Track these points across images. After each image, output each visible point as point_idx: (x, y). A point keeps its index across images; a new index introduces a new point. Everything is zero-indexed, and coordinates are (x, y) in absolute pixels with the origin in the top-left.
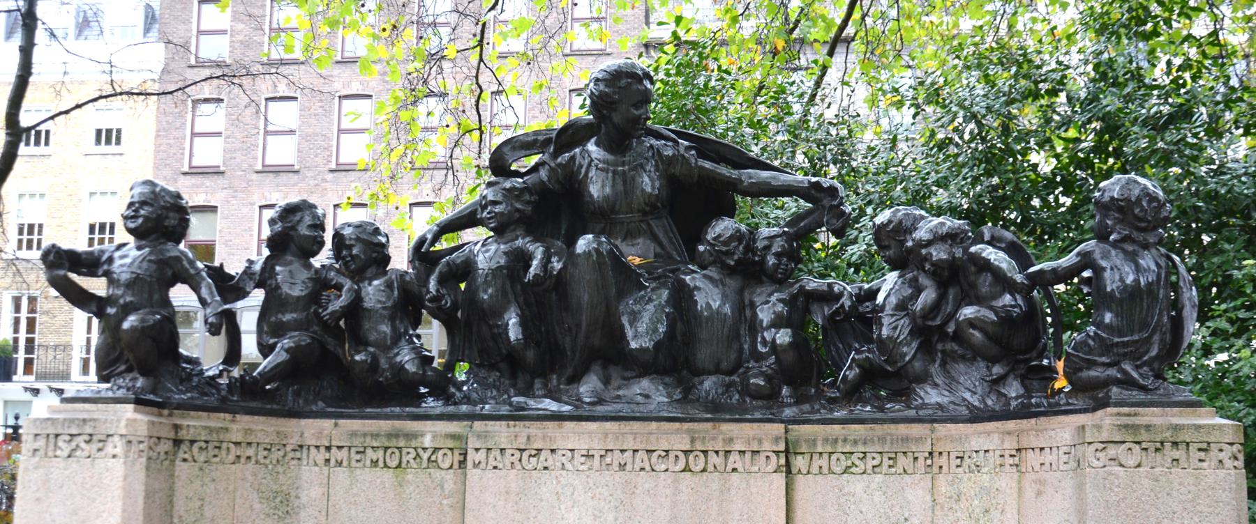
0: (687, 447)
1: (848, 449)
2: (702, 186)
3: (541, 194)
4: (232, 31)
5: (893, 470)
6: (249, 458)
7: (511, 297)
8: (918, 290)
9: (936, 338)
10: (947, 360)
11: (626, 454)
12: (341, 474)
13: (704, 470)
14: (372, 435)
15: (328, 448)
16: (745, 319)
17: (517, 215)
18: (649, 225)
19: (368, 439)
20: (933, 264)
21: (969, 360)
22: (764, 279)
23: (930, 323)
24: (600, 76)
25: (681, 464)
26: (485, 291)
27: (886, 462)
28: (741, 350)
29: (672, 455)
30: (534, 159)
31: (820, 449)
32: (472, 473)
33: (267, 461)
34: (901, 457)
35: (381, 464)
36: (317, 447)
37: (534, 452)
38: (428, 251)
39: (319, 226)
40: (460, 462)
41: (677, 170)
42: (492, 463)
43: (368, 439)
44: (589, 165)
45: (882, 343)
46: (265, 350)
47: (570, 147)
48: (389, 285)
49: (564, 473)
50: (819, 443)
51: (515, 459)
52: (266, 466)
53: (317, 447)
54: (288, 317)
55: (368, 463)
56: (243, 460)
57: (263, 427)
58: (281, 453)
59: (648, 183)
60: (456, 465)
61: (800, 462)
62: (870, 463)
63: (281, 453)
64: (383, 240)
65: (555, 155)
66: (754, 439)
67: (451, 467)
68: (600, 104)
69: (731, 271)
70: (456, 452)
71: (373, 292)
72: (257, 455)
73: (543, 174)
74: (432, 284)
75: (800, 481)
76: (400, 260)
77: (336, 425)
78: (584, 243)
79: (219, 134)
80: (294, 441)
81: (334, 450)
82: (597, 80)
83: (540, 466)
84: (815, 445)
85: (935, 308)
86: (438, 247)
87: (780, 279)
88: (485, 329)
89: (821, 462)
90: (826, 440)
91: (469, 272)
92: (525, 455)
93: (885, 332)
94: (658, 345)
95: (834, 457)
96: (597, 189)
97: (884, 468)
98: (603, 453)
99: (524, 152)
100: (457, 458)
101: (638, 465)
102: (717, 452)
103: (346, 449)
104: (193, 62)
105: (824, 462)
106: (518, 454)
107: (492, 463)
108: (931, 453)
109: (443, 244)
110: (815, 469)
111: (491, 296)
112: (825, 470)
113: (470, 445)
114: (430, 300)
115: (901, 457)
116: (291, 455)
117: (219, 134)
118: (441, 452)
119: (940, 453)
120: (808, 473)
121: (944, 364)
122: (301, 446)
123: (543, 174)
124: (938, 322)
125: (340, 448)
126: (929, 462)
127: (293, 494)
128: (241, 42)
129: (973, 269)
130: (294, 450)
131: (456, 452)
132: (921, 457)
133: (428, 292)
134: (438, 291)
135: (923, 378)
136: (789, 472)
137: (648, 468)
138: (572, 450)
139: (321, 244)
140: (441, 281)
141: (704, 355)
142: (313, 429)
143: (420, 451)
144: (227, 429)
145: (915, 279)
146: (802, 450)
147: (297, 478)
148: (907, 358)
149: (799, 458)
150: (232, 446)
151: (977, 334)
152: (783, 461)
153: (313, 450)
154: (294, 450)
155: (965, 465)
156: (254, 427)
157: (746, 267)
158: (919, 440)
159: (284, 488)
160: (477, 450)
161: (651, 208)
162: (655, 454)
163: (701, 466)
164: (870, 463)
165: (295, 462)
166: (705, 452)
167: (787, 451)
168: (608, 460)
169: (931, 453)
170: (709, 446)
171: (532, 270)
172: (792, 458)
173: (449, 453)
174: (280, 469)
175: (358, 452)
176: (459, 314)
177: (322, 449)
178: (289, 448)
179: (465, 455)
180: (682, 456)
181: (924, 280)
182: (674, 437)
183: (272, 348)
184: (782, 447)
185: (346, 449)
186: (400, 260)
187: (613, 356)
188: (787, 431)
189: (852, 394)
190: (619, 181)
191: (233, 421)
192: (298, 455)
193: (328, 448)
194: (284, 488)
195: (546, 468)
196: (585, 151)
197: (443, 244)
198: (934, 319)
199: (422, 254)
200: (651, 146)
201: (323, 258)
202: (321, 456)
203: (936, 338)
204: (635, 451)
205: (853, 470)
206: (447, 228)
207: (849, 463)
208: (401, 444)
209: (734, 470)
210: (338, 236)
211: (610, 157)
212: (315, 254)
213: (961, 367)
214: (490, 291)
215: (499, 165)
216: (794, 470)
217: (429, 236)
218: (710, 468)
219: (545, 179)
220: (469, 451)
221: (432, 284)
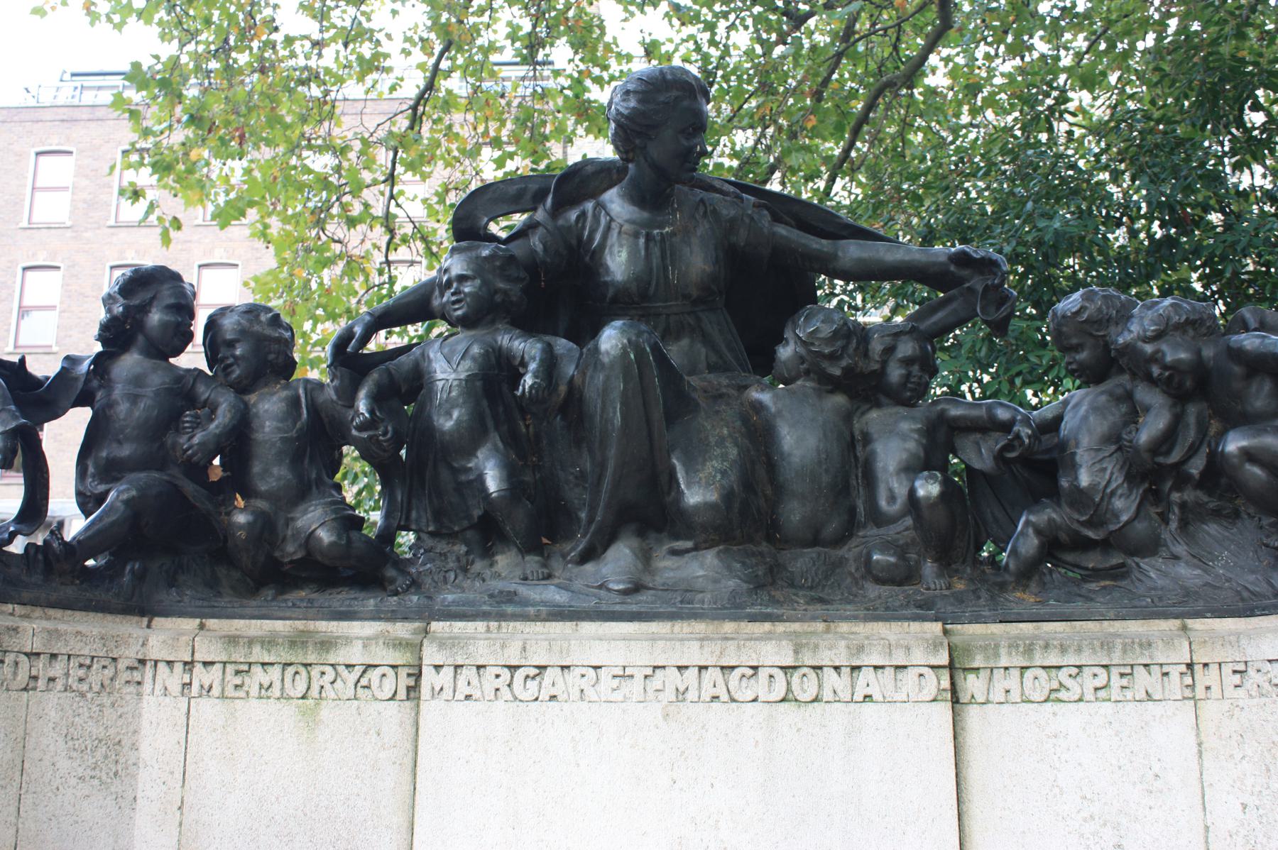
0: (789, 661)
1: (1053, 660)
2: (761, 272)
3: (530, 267)
4: (74, 188)
5: (1129, 694)
6: (52, 680)
7: (490, 423)
8: (1134, 413)
9: (1169, 484)
10: (1190, 518)
11: (687, 673)
12: (206, 710)
13: (816, 700)
14: (262, 643)
15: (188, 665)
16: (851, 464)
17: (498, 298)
18: (698, 319)
19: (257, 649)
20: (1165, 367)
21: (1227, 517)
22: (883, 399)
23: (1161, 459)
24: (631, 87)
25: (779, 690)
26: (449, 414)
27: (1116, 681)
28: (852, 511)
29: (763, 673)
30: (518, 219)
31: (1004, 662)
32: (430, 708)
33: (85, 687)
34: (1140, 672)
35: (276, 691)
36: (170, 663)
37: (533, 671)
38: (356, 354)
39: (184, 308)
40: (409, 689)
41: (741, 237)
42: (463, 690)
43: (257, 649)
44: (608, 228)
45: (1080, 498)
46: (87, 502)
47: (575, 201)
48: (294, 402)
49: (584, 705)
50: (1003, 651)
51: (500, 683)
52: (83, 695)
53: (170, 663)
54: (125, 451)
55: (254, 691)
56: (41, 684)
57: (85, 631)
58: (109, 673)
59: (697, 261)
60: (402, 694)
61: (972, 685)
62: (1090, 683)
63: (109, 673)
64: (287, 335)
65: (556, 211)
66: (898, 646)
67: (392, 698)
68: (631, 132)
69: (830, 384)
70: (403, 672)
71: (269, 407)
72: (67, 675)
73: (536, 241)
74: (362, 406)
75: (973, 716)
76: (313, 363)
77: (202, 627)
78: (611, 339)
79: (53, 308)
80: (130, 653)
81: (198, 668)
82: (627, 92)
83: (544, 695)
84: (997, 655)
85: (1167, 439)
86: (372, 347)
87: (910, 394)
88: (445, 475)
89: (1007, 684)
90: (1013, 646)
91: (421, 387)
92: (520, 674)
93: (1084, 479)
94: (728, 497)
95: (1029, 674)
96: (618, 262)
97: (1115, 693)
98: (649, 671)
99: (506, 208)
100: (404, 681)
101: (707, 693)
102: (836, 668)
103: (218, 667)
104: (25, 224)
105: (1013, 681)
106: (506, 674)
107: (463, 690)
108: (1190, 666)
109: (381, 341)
110: (998, 695)
111: (458, 422)
112: (1015, 695)
113: (426, 661)
114: (360, 428)
115: (1140, 672)
116: (126, 676)
117: (53, 308)
118: (379, 671)
119: (1206, 665)
120: (987, 702)
121: (1184, 524)
122: (142, 662)
123: (536, 241)
124: (1175, 457)
125: (206, 664)
126: (1188, 680)
127: (126, 742)
128: (85, 201)
129: (1237, 369)
130: (131, 668)
131: (403, 672)
132: (1175, 672)
133: (357, 413)
134: (371, 412)
135: (1151, 547)
136: (955, 700)
137: (725, 697)
138: (596, 668)
139: (189, 337)
140: (377, 399)
141: (794, 513)
142: (166, 636)
143: (341, 669)
144: (16, 630)
145: (1129, 397)
146: (975, 665)
147: (137, 715)
148: (1124, 518)
149: (971, 677)
150: (23, 658)
151: (1257, 470)
152: (946, 683)
153: (161, 666)
154: (131, 668)
155: (1248, 685)
156: (62, 627)
157: (858, 377)
158: (1169, 642)
159: (111, 731)
160: (438, 668)
161: (705, 297)
162: (737, 672)
163: (811, 693)
164: (1090, 683)
165: (132, 689)
166: (818, 668)
167: (951, 667)
168: (656, 682)
169: (1190, 666)
170: (825, 658)
171: (528, 380)
172: (959, 676)
173: (390, 672)
174: (106, 700)
175: (238, 672)
176: (403, 452)
177: (179, 668)
178: (122, 665)
179: (418, 676)
180: (779, 675)
181: (1144, 394)
182: (767, 645)
183: (101, 499)
184: (944, 660)
185: (218, 667)
186: (313, 363)
187: (649, 513)
188: (945, 632)
189: (1028, 572)
190: (656, 251)
191: (26, 617)
192: (137, 676)
193: (188, 665)
194: (111, 731)
195: (553, 698)
196: (601, 206)
197: (381, 341)
198: (1168, 453)
199: (348, 357)
200: (702, 201)
201: (193, 358)
202: (174, 679)
203: (1169, 484)
204: (702, 668)
205: (1063, 695)
206: (388, 318)
207: (1055, 685)
208: (311, 658)
209: (867, 697)
210: (212, 325)
211: (646, 215)
212: (178, 351)
213: (1213, 529)
214: (456, 414)
215: (467, 227)
216: (964, 698)
217: (358, 330)
218: (827, 695)
219: (539, 248)
220: (424, 669)
221: (362, 406)
